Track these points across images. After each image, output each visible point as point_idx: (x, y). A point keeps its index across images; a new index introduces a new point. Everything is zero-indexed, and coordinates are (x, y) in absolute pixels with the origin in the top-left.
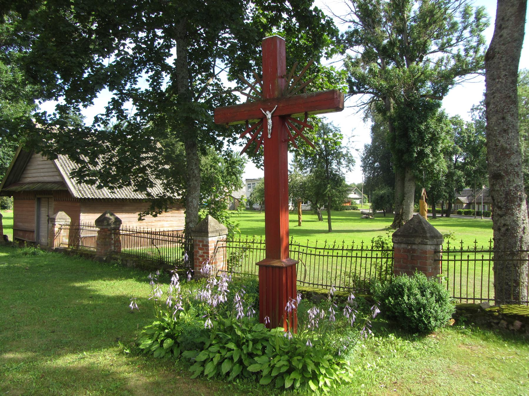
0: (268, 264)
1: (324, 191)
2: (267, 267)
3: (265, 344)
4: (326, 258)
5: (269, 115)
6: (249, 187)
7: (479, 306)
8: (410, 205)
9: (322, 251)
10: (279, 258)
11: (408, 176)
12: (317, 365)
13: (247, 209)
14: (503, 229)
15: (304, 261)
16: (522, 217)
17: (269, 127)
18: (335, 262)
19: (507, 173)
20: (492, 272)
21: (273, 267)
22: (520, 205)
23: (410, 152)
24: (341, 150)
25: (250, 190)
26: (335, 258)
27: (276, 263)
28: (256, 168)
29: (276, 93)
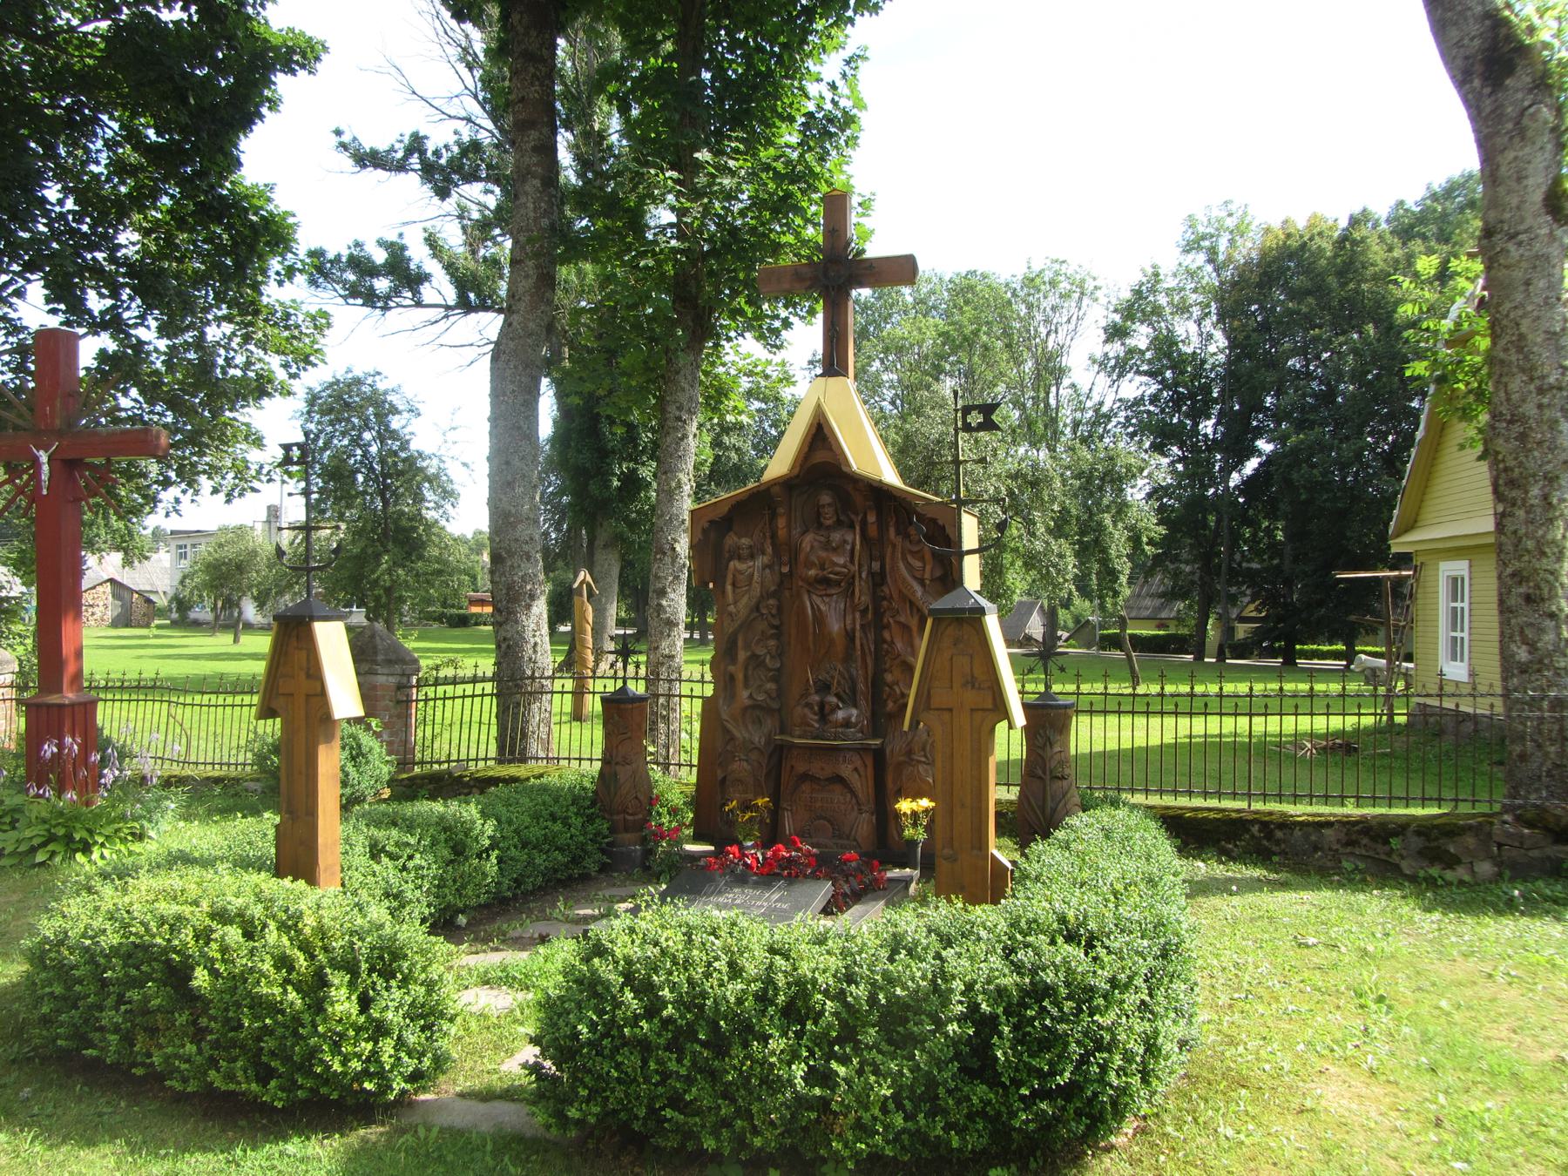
0: (39, 700)
1: (373, 572)
2: (38, 706)
3: (16, 816)
4: (220, 709)
5: (44, 457)
6: (183, 556)
7: (449, 772)
8: (605, 609)
9: (213, 697)
10: (59, 690)
11: (603, 536)
12: (91, 832)
13: (175, 624)
14: (504, 646)
15: (179, 718)
16: (532, 626)
17: (45, 477)
18: (220, 716)
19: (511, 554)
20: (494, 720)
21: (49, 706)
22: (529, 607)
23: (604, 475)
24: (424, 464)
25: (185, 564)
26: (228, 710)
27: (54, 699)
28: (1357, 210)
29: (58, 422)
